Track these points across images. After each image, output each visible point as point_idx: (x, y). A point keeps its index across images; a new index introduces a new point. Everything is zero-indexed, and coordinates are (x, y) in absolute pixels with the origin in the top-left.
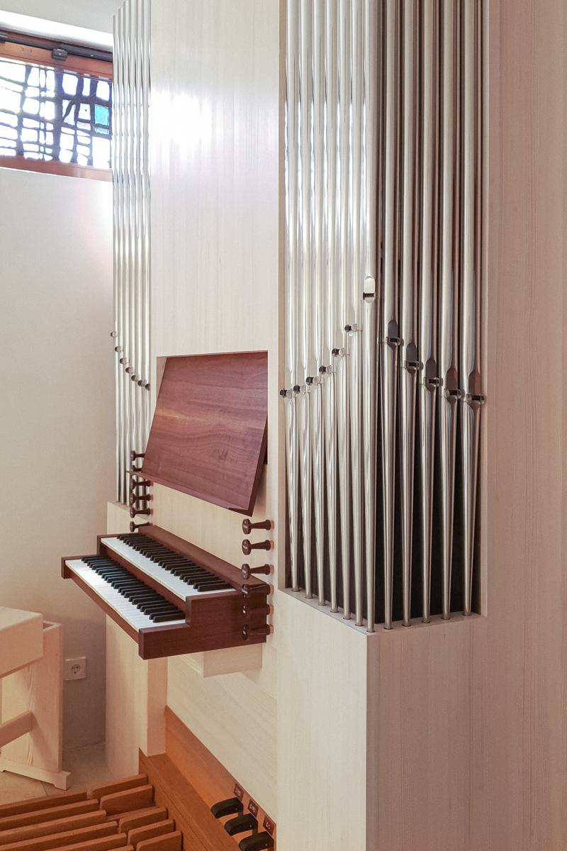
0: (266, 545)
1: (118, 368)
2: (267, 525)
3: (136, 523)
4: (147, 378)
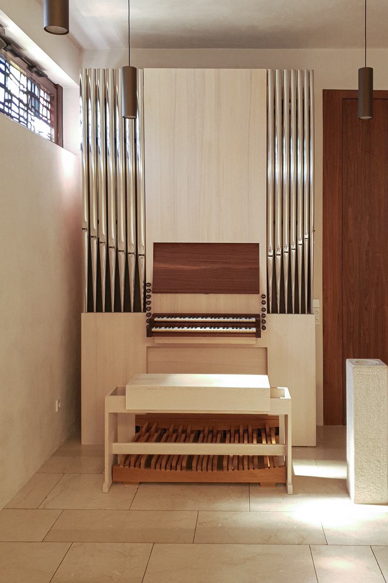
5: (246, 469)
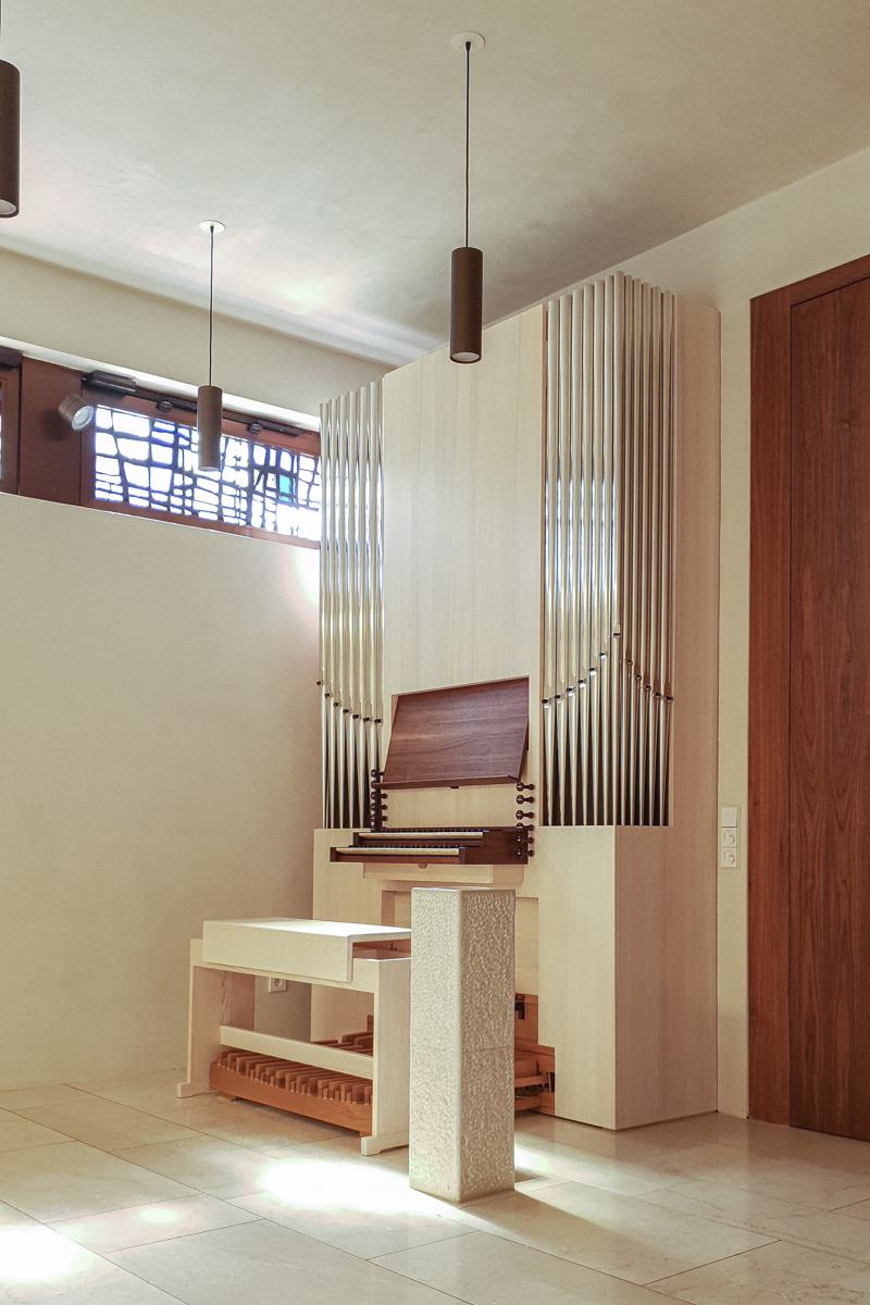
0: (531, 800)
2: (531, 787)
5: (343, 1101)
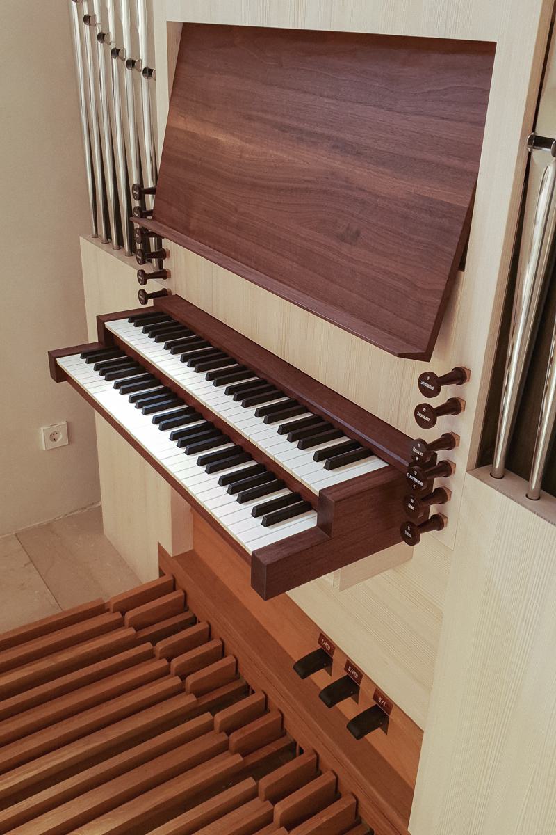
1: (82, 36)
3: (148, 292)
4: (143, 55)
